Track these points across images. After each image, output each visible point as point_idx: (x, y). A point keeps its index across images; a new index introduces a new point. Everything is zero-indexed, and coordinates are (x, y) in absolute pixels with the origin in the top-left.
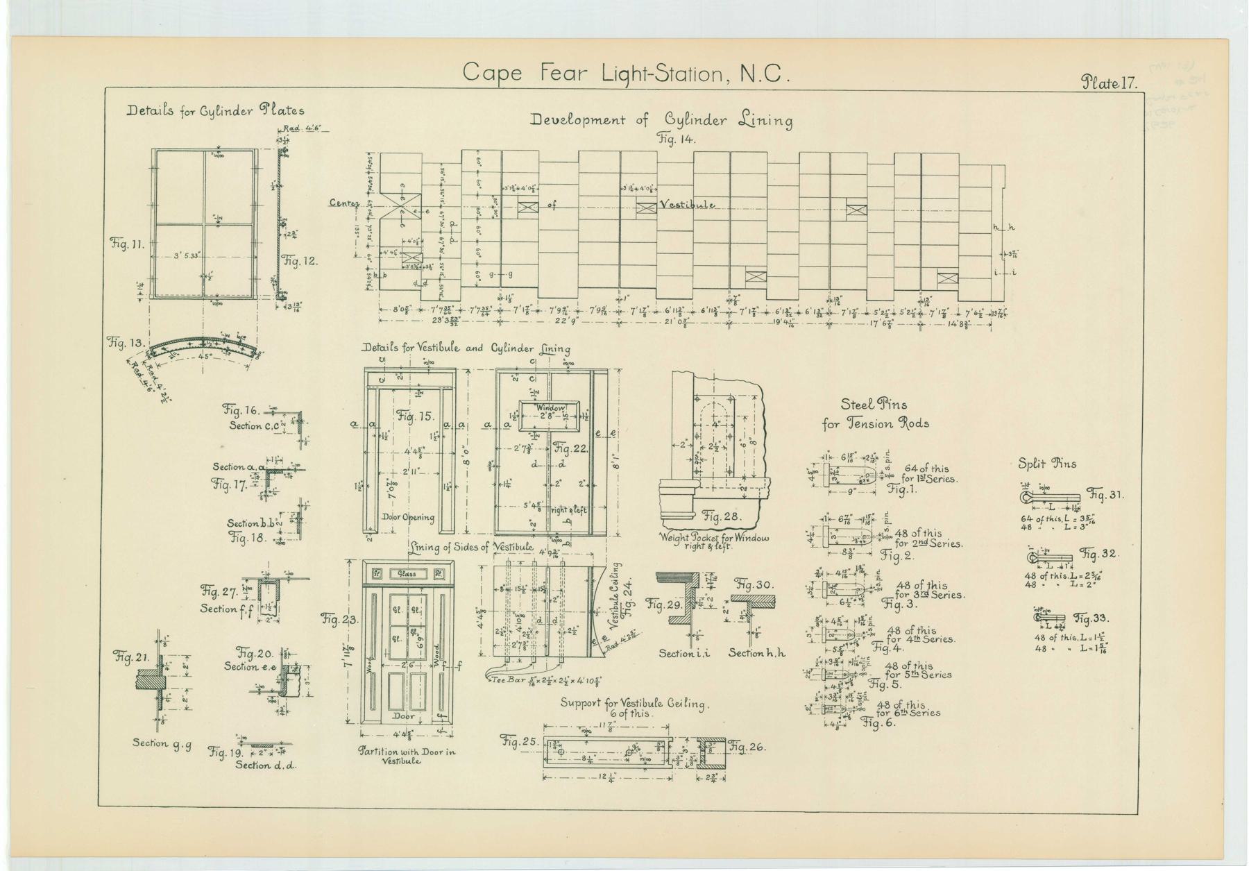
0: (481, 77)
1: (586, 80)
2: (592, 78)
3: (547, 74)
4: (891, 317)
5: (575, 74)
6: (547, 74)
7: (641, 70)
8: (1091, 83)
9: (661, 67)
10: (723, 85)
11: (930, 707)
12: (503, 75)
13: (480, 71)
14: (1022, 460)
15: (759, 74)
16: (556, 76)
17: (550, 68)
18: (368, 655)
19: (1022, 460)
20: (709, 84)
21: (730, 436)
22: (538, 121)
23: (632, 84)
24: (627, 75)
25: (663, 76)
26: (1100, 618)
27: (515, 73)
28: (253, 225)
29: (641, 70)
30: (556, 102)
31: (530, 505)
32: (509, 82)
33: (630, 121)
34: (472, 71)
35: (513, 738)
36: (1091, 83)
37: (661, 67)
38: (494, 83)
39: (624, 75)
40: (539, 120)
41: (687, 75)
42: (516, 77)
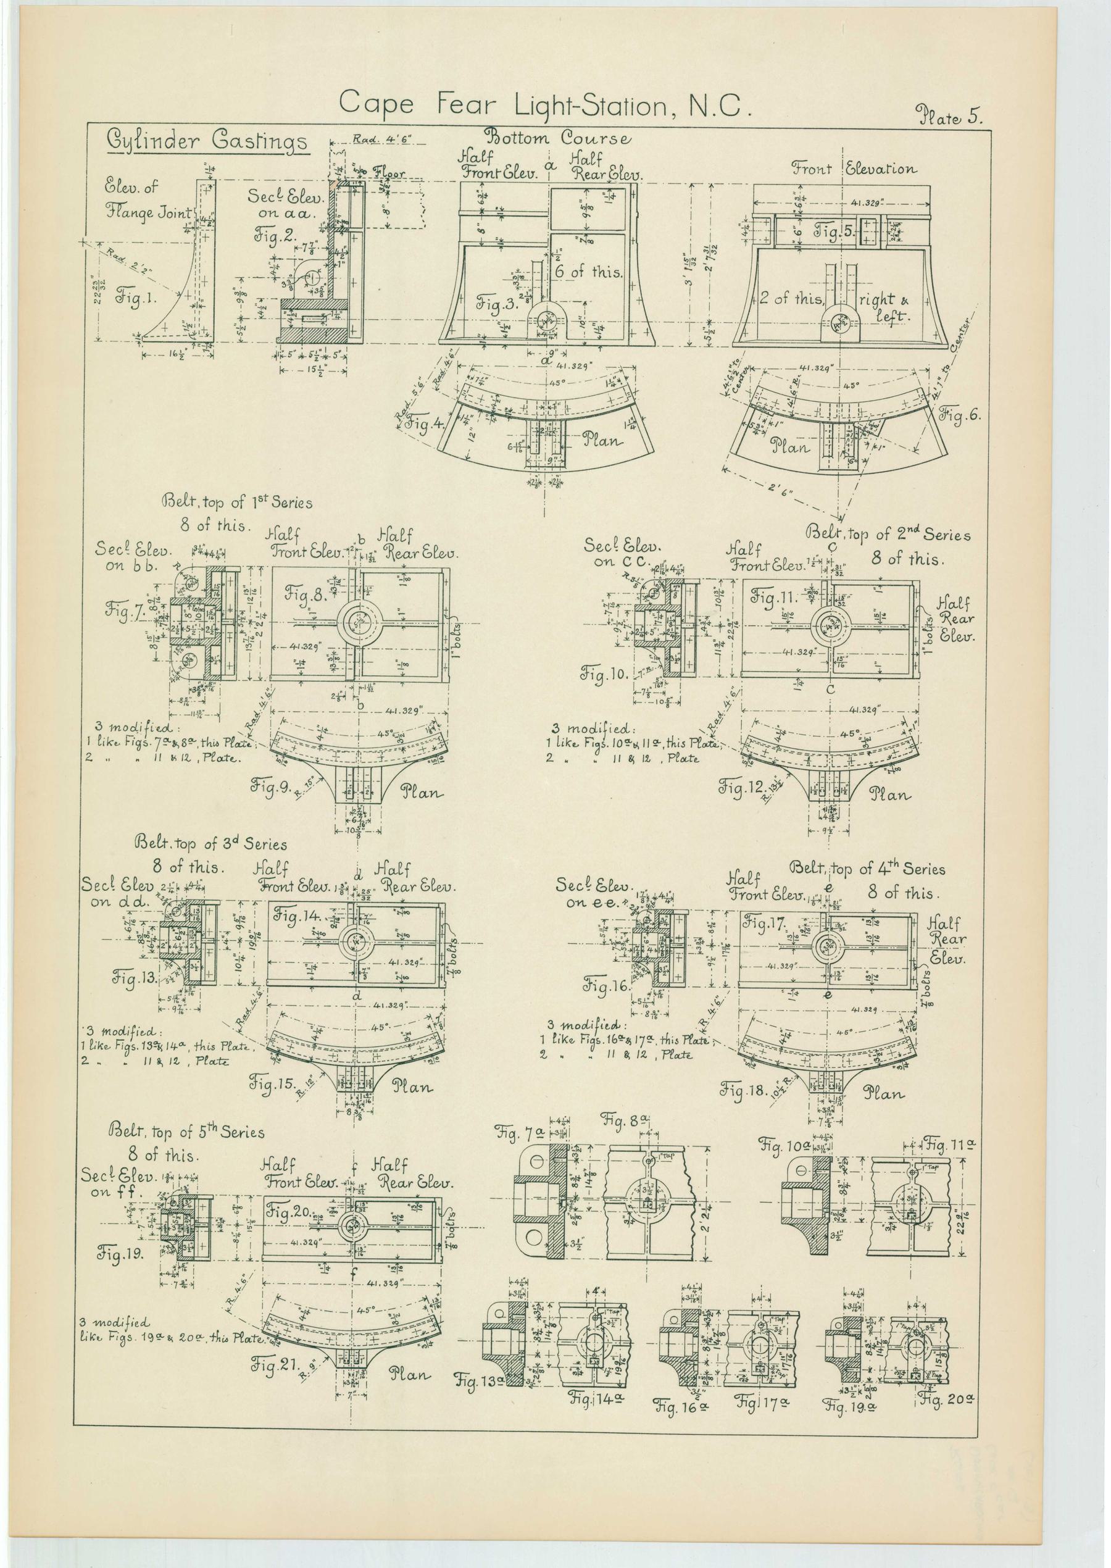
0: (362, 107)
3: (446, 106)
4: (321, 361)
6: (446, 106)
7: (565, 101)
9: (589, 97)
10: (668, 121)
11: (444, 548)
12: (390, 106)
13: (361, 101)
14: (588, 540)
15: (713, 107)
17: (450, 98)
19: (588, 540)
20: (649, 120)
21: (345, 228)
25: (592, 109)
27: (405, 105)
29: (565, 101)
31: (125, 1060)
32: (396, 117)
34: (350, 101)
38: (378, 117)
39: (543, 108)
42: (405, 108)
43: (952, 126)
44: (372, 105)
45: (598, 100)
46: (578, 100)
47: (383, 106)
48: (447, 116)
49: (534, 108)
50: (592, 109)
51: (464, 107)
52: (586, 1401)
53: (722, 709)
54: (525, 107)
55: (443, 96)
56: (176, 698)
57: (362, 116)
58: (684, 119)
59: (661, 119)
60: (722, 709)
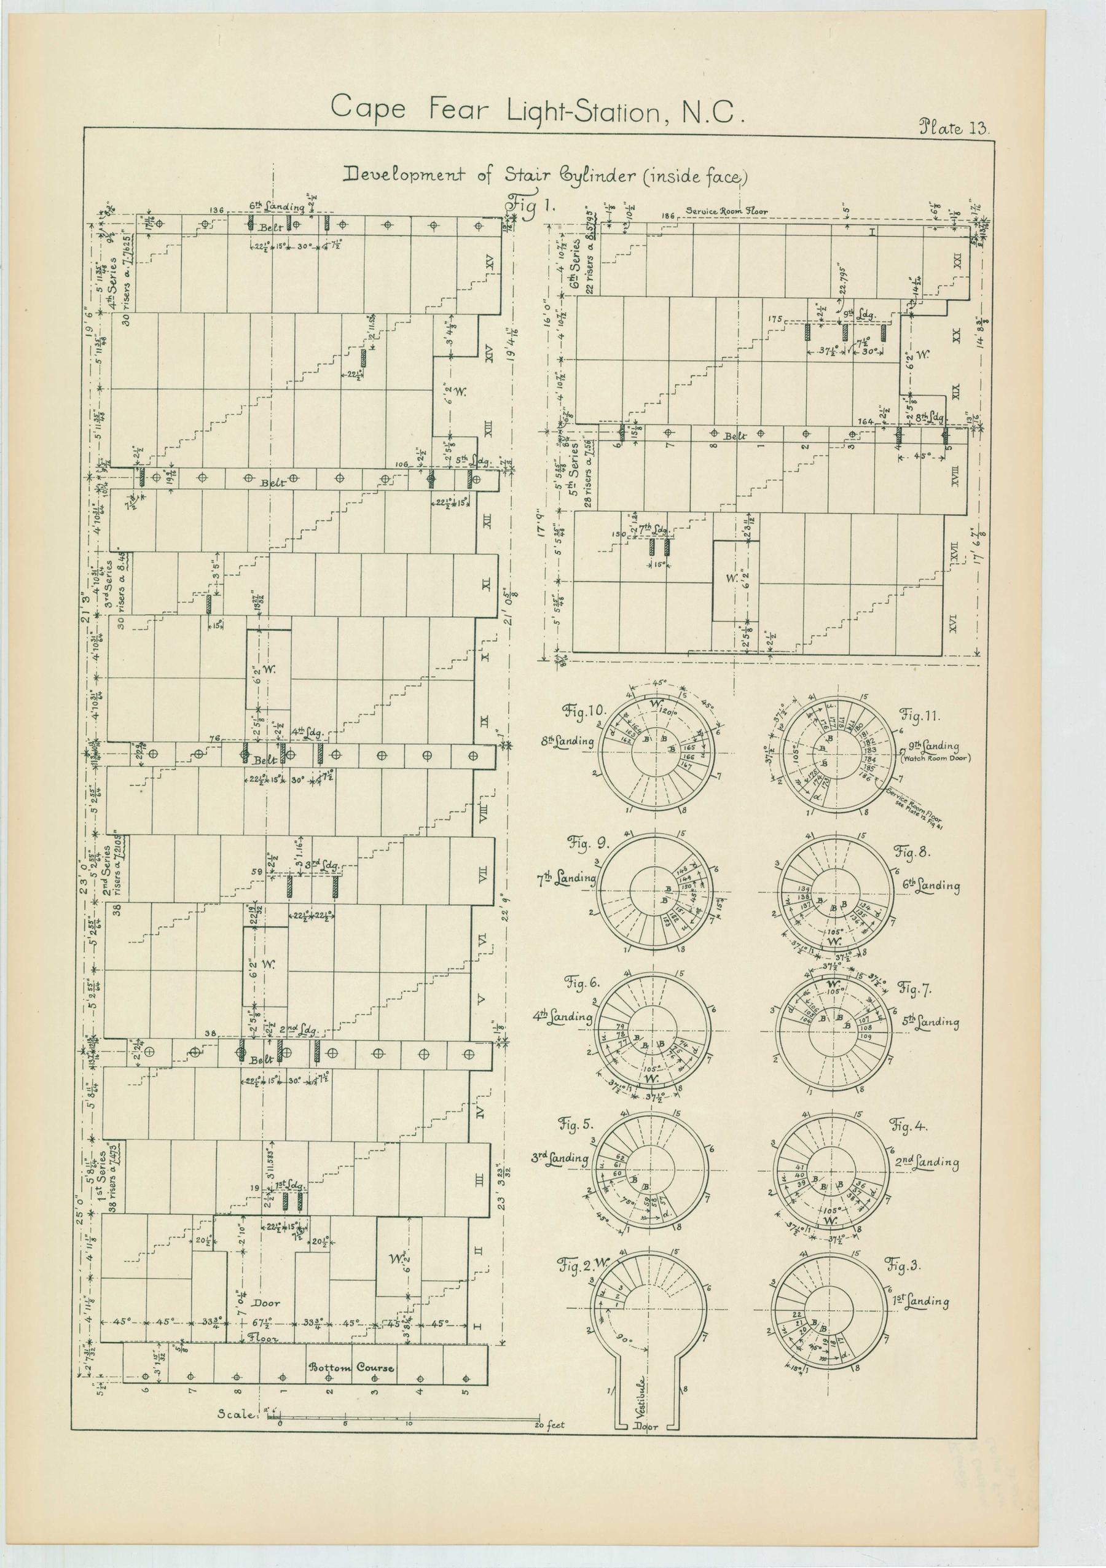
0: (354, 111)
1: (487, 121)
2: (494, 118)
3: (438, 110)
5: (475, 111)
6: (438, 110)
8: (930, 127)
9: (582, 103)
10: (660, 127)
12: (382, 110)
15: (706, 113)
16: (447, 113)
17: (442, 103)
18: (530, 1427)
22: (353, 176)
23: (546, 126)
24: (540, 113)
25: (585, 115)
26: (931, 715)
27: (397, 110)
28: (711, 653)
30: (370, 151)
33: (470, 178)
34: (342, 105)
35: (574, 1262)
36: (930, 127)
37: (582, 103)
38: (369, 122)
39: (535, 113)
40: (354, 174)
41: (616, 113)
44: (364, 110)
45: (591, 106)
46: (570, 106)
49: (527, 114)
50: (585, 115)
51: (456, 112)
54: (517, 112)
55: (435, 101)
58: (677, 126)
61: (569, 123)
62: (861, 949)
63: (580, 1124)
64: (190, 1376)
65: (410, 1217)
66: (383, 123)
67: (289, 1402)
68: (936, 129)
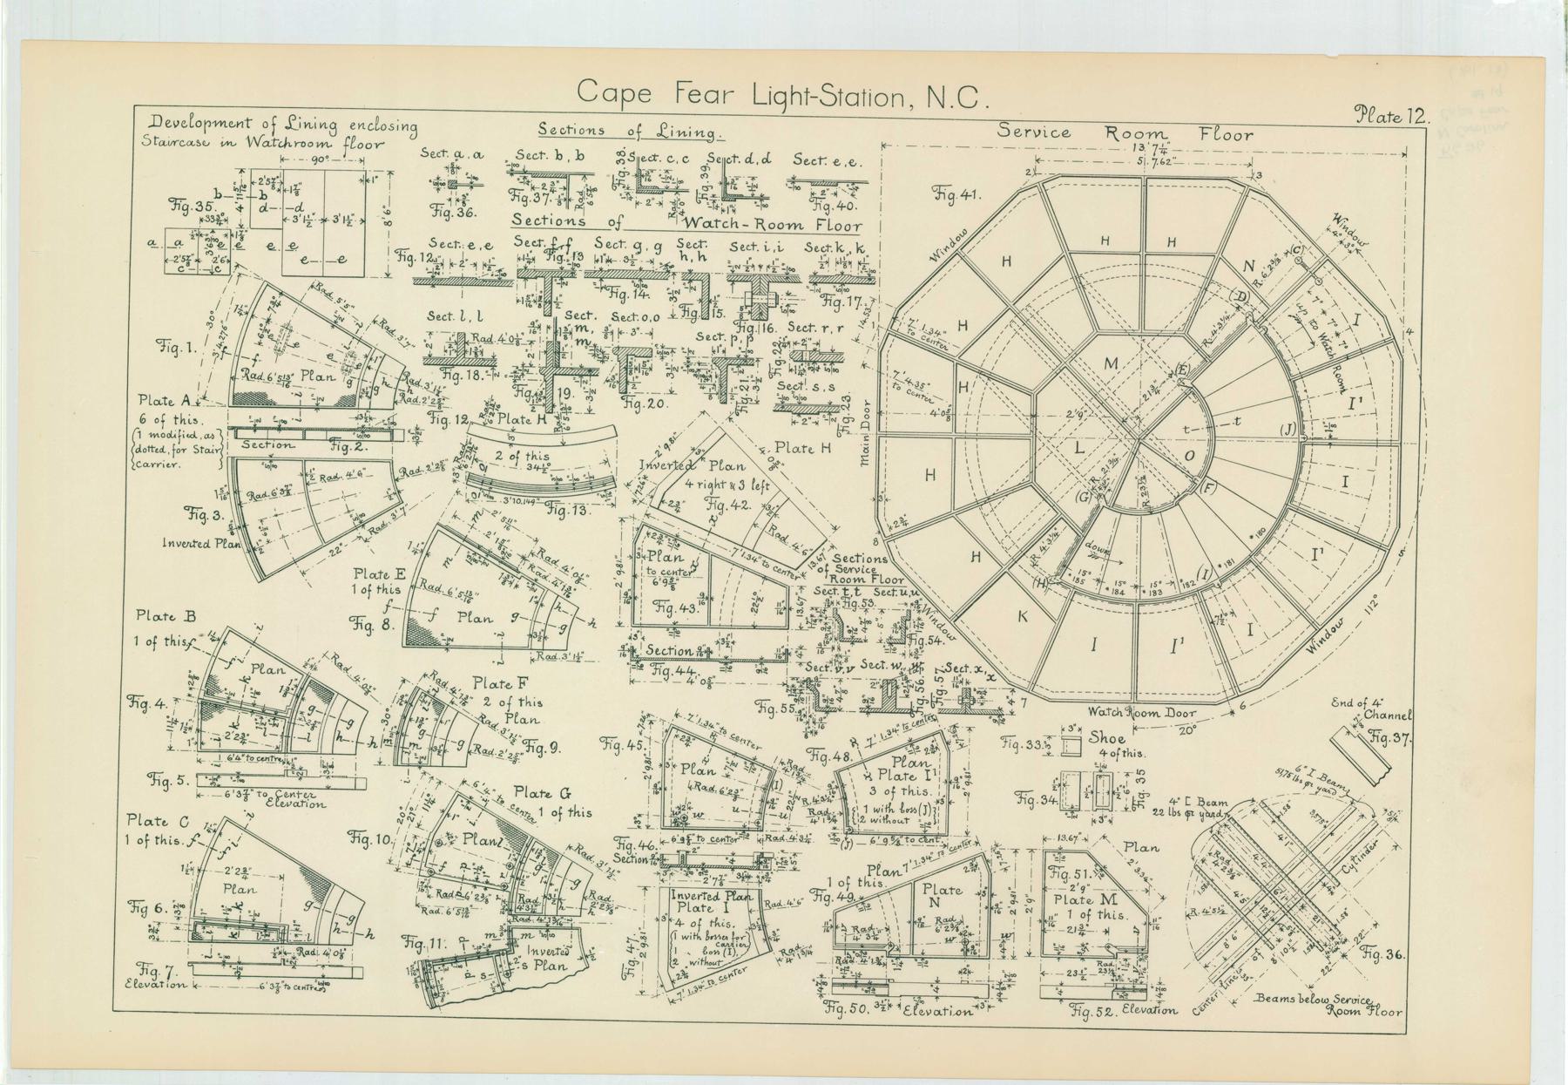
1: (735, 104)
2: (740, 101)
3: (684, 95)
5: (720, 96)
6: (684, 95)
7: (802, 92)
9: (827, 88)
10: (905, 112)
12: (628, 95)
13: (599, 90)
15: (951, 98)
17: (687, 88)
20: (887, 111)
24: (784, 99)
25: (829, 99)
27: (643, 94)
29: (802, 92)
37: (827, 88)
38: (616, 106)
39: (780, 98)
41: (862, 98)
42: (644, 98)
43: (1392, 124)
44: (610, 95)
47: (620, 96)
48: (685, 106)
49: (772, 98)
52: (667, 673)
53: (353, 673)
54: (762, 96)
56: (586, 404)
57: (600, 104)
59: (898, 111)
60: (353, 673)
61: (814, 107)
62: (278, 960)
63: (173, 780)
64: (976, 556)
65: (754, 627)
66: (628, 107)
67: (355, 692)
68: (1374, 118)
